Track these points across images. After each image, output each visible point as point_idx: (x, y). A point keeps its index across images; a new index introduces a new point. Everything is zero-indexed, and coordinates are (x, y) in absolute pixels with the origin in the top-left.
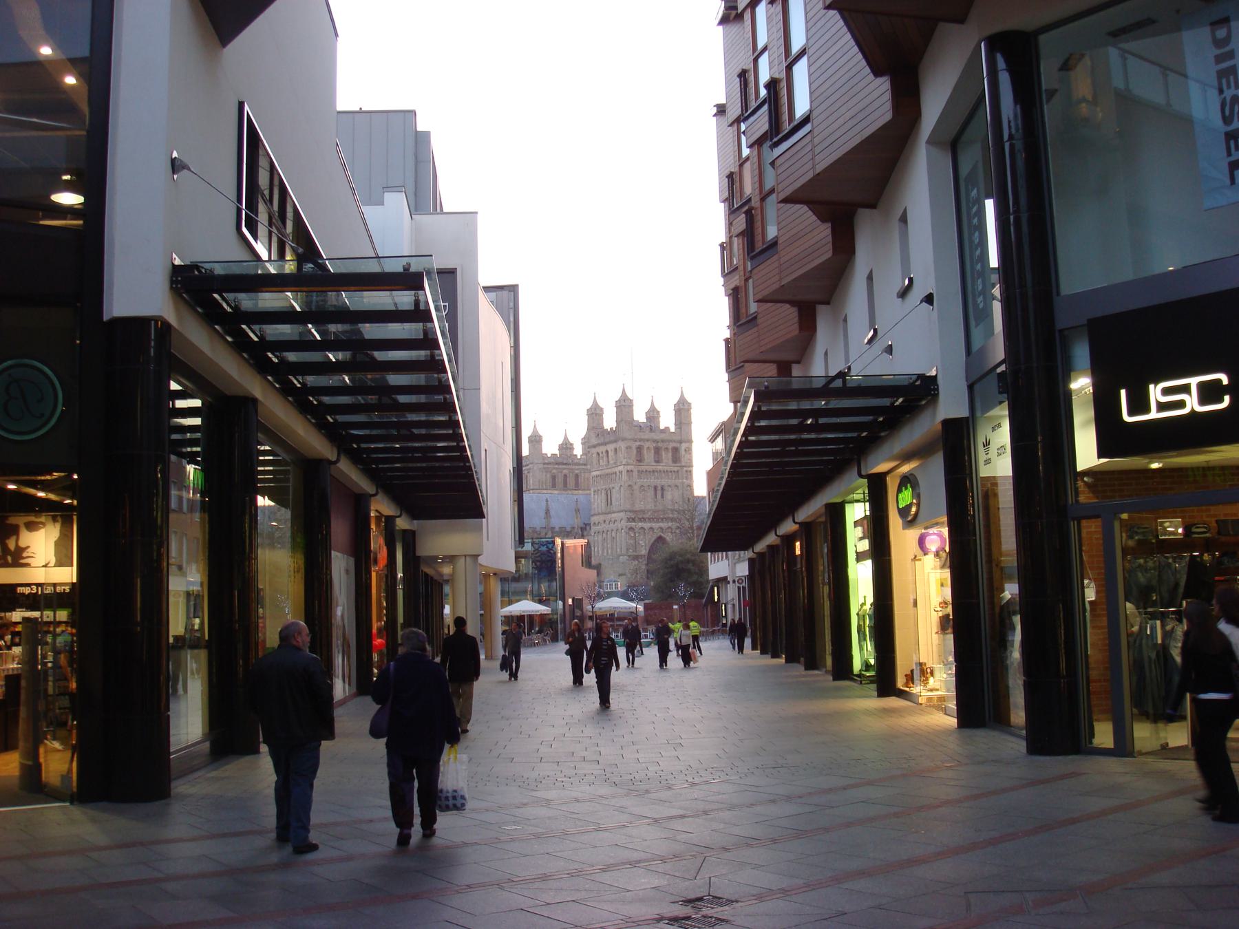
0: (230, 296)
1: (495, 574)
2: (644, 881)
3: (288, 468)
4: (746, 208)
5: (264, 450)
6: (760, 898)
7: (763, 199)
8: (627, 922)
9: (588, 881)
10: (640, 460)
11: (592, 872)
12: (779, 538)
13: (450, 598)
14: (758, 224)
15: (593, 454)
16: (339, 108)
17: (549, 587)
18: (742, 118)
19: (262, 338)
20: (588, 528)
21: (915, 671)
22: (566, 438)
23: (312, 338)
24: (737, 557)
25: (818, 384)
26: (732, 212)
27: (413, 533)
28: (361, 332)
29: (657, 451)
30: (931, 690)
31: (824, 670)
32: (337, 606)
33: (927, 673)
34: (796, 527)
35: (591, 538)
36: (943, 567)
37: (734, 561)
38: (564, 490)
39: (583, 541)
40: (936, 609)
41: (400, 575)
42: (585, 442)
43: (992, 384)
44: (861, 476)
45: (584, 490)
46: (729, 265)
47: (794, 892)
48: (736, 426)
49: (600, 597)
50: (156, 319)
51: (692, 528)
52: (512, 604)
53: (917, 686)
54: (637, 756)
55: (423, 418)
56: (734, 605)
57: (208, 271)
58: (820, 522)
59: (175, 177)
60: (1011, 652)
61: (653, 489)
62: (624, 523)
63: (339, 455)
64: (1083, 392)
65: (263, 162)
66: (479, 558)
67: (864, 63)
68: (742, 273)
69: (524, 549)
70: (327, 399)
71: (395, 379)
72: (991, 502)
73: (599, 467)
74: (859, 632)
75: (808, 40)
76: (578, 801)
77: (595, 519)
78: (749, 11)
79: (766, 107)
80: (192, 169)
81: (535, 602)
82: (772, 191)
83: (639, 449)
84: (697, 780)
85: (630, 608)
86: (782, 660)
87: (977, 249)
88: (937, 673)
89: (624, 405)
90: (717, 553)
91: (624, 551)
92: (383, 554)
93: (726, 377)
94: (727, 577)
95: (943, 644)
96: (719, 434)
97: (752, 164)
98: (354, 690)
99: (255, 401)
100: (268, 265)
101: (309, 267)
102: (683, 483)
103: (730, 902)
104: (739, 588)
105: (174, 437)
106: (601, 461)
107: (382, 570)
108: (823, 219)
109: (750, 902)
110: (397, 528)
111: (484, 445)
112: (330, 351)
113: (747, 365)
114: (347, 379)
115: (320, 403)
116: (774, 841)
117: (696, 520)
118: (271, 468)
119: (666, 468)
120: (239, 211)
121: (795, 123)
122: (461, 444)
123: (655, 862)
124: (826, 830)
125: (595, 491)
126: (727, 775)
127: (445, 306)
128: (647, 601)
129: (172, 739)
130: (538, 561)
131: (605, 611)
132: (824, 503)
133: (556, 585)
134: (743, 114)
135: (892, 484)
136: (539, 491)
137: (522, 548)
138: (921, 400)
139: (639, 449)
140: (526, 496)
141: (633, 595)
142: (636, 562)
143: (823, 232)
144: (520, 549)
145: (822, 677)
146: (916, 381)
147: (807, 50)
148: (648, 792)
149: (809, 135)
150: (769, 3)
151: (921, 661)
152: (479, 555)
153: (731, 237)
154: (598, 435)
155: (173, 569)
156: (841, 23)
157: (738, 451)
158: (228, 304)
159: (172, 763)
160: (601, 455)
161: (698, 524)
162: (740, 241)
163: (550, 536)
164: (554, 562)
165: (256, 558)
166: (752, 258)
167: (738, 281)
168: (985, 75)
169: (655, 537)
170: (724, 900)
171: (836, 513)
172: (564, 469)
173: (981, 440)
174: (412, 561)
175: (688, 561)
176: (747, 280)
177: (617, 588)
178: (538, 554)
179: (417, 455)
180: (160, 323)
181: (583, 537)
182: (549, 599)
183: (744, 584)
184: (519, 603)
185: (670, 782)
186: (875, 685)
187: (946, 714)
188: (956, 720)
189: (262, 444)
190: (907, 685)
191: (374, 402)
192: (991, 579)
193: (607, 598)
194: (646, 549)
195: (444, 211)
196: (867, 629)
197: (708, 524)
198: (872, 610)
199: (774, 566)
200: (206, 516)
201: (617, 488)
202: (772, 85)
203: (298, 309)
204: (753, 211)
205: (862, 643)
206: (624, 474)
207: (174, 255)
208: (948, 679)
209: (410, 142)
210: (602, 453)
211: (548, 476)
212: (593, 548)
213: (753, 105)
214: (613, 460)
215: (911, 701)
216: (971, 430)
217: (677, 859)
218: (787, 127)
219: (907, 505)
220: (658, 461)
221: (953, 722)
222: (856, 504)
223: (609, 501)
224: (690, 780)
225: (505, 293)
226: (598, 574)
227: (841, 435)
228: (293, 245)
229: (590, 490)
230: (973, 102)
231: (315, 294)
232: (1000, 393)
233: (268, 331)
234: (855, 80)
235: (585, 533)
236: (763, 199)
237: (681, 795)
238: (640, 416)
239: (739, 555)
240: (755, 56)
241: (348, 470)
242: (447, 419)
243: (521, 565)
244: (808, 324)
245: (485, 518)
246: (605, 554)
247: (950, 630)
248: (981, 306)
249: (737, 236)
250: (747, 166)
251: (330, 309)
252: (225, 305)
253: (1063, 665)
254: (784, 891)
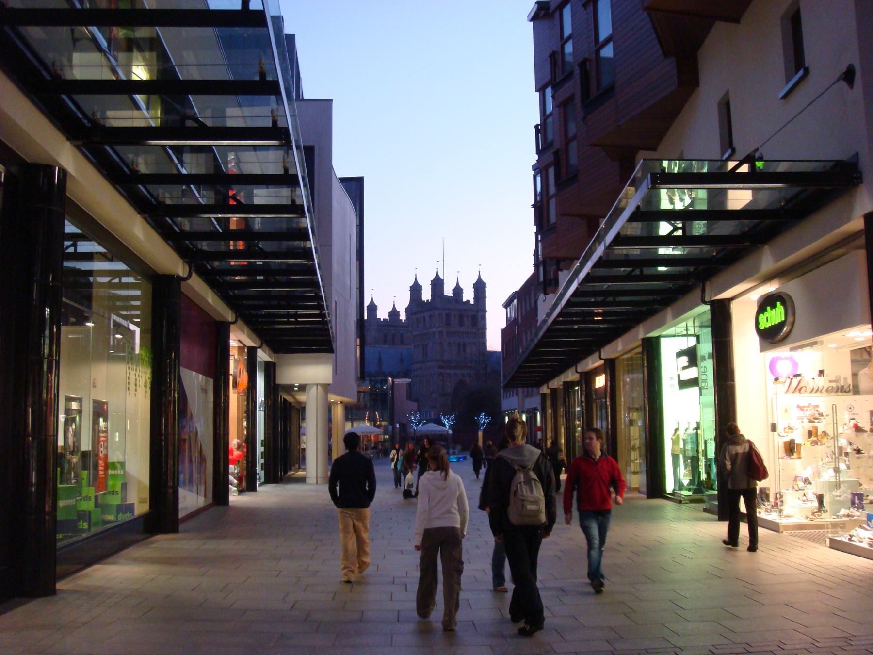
10: (448, 324)
29: (461, 317)
42: (408, 310)
83: (448, 316)
89: (437, 284)
92: (244, 380)
98: (210, 500)
111: (335, 297)
139: (448, 316)
199: (569, 399)
219: (775, 325)
238: (448, 291)
252: (44, 73)
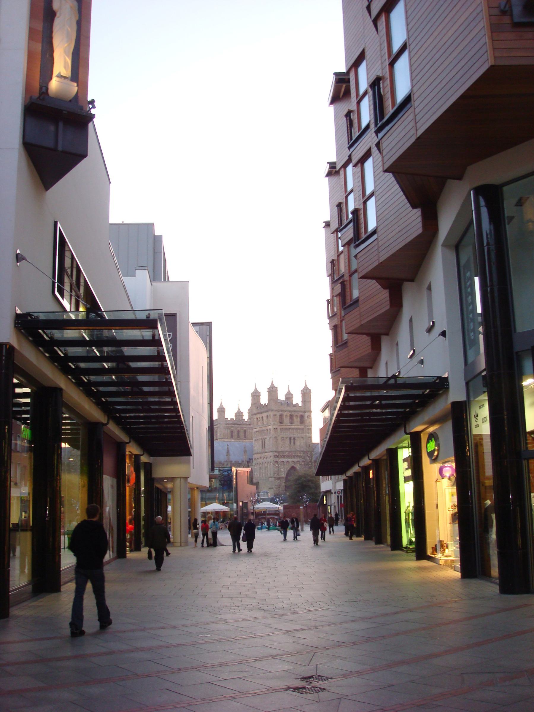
0: (48, 331)
1: (197, 488)
2: (279, 667)
3: (80, 427)
4: (341, 281)
5: (66, 417)
6: (345, 676)
7: (351, 276)
8: (269, 690)
9: (248, 667)
11: (250, 661)
12: (360, 468)
13: (172, 501)
14: (348, 290)
15: (254, 419)
16: (111, 222)
17: (229, 495)
18: (339, 230)
19: (66, 354)
20: (251, 461)
21: (437, 545)
22: (239, 410)
23: (95, 355)
24: (337, 478)
25: (382, 382)
26: (334, 282)
27: (150, 464)
28: (123, 352)
29: (291, 417)
30: (447, 556)
31: (386, 544)
32: (106, 506)
33: (444, 547)
34: (370, 462)
35: (253, 467)
36: (453, 486)
37: (335, 481)
38: (237, 439)
39: (248, 469)
40: (449, 510)
41: (143, 488)
42: (250, 411)
43: (480, 380)
44: (406, 433)
45: (249, 439)
46: (332, 312)
47: (365, 673)
48: (335, 405)
49: (258, 501)
50: (6, 344)
51: (311, 461)
52: (207, 505)
53: (438, 554)
54: (277, 594)
55: (157, 399)
56: (335, 506)
57: (36, 317)
58: (384, 459)
59: (18, 264)
60: (491, 535)
61: (289, 439)
62: (272, 459)
63: (108, 420)
64: (530, 387)
65: (67, 254)
66: (188, 479)
67: (406, 201)
68: (339, 317)
69: (214, 473)
70: (102, 389)
71: (141, 378)
72: (479, 449)
73: (258, 426)
74: (406, 522)
75: (375, 187)
76: (243, 620)
77: (255, 456)
78: (343, 169)
79: (352, 224)
80: (28, 260)
81: (221, 504)
82: (356, 271)
83: (281, 416)
84: (311, 609)
85: (275, 508)
86: (362, 539)
87: (470, 306)
88: (450, 547)
89: (272, 391)
90: (325, 476)
91: (272, 475)
92: (133, 476)
93: (330, 375)
94: (331, 490)
95: (453, 530)
96: (326, 408)
97: (345, 256)
98: (115, 555)
99: (61, 389)
100: (71, 314)
101: (93, 315)
102: (306, 435)
103: (328, 678)
104: (338, 497)
105: (14, 409)
106: (259, 423)
107: (132, 486)
108: (384, 287)
109: (339, 679)
110: (141, 462)
112: (104, 362)
113: (342, 369)
114: (114, 377)
115: (98, 391)
116: (354, 644)
117: (314, 457)
118: (69, 427)
119: (296, 427)
120: (54, 283)
121: (368, 234)
122: (178, 414)
123: (286, 656)
124: (384, 637)
125: (255, 440)
126: (328, 605)
127: (169, 335)
128: (285, 504)
129: (11, 583)
130: (222, 480)
131: (261, 510)
132: (386, 448)
133: (232, 494)
134: (339, 228)
135: (424, 438)
136: (223, 440)
137: (213, 473)
138: (440, 390)
140: (216, 443)
141: (277, 500)
142: (279, 481)
143: (385, 295)
144: (212, 474)
145: (385, 549)
146: (436, 380)
147: (375, 193)
148: (283, 615)
149: (376, 240)
150: (354, 166)
151: (440, 540)
152: (188, 477)
153: (333, 296)
154: (257, 408)
155: (12, 483)
156: (393, 179)
157: (336, 419)
158: (47, 336)
159: (10, 597)
160: (259, 419)
161: (315, 459)
162: (338, 298)
163: (229, 466)
164: (231, 481)
165: (61, 479)
166: (345, 309)
167: (337, 321)
168: (473, 208)
169: (290, 467)
170: (325, 678)
171: (393, 454)
172: (239, 427)
173: (473, 414)
174: (150, 480)
175: (309, 481)
176: (341, 321)
177: (268, 496)
178: (223, 476)
179: (153, 420)
180: (8, 346)
181: (248, 466)
182: (228, 503)
183: (341, 494)
184: (211, 504)
185: (296, 610)
186: (415, 553)
187: (455, 570)
188: (460, 574)
189: (64, 414)
190: (433, 553)
191: (128, 390)
192: (479, 493)
193: (262, 502)
194: (284, 473)
195: (170, 280)
196: (411, 521)
197: (320, 459)
198: (413, 510)
200: (32, 454)
201: (268, 438)
202: (355, 212)
203: (87, 339)
204: (345, 283)
205: (408, 529)
206: (272, 430)
207: (17, 308)
208: (456, 550)
209: (151, 241)
210: (260, 418)
211: (229, 431)
212: (254, 473)
213: (345, 222)
214: (266, 422)
215: (436, 563)
216: (468, 407)
217: (298, 654)
218: (364, 236)
220: (291, 423)
221: (458, 574)
222: (404, 449)
223: (263, 446)
224: (307, 608)
225: (204, 327)
226: (257, 488)
227: (395, 410)
228: (84, 303)
229: (253, 439)
231: (95, 330)
232: (484, 387)
233: (69, 351)
234: (401, 210)
235: (250, 464)
236: (351, 276)
237: (302, 617)
238: (281, 397)
239: (338, 477)
240: (346, 195)
241: (113, 428)
242: (171, 400)
243: (212, 483)
244: (376, 346)
245: (191, 456)
246: (261, 477)
247: (457, 522)
248: (472, 338)
249: (336, 296)
250: (342, 256)
251: (104, 339)
252: (45, 336)
253: (520, 542)
254: (359, 673)
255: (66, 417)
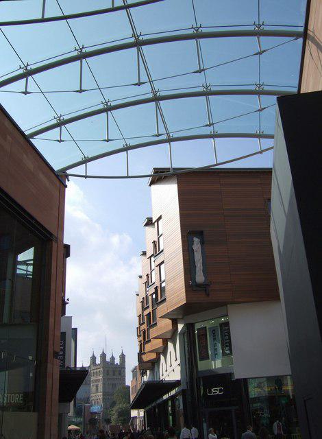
29: (114, 372)
89: (103, 356)
197: (54, 264)
230: (210, 311)
238: (108, 359)
255: (172, 410)
